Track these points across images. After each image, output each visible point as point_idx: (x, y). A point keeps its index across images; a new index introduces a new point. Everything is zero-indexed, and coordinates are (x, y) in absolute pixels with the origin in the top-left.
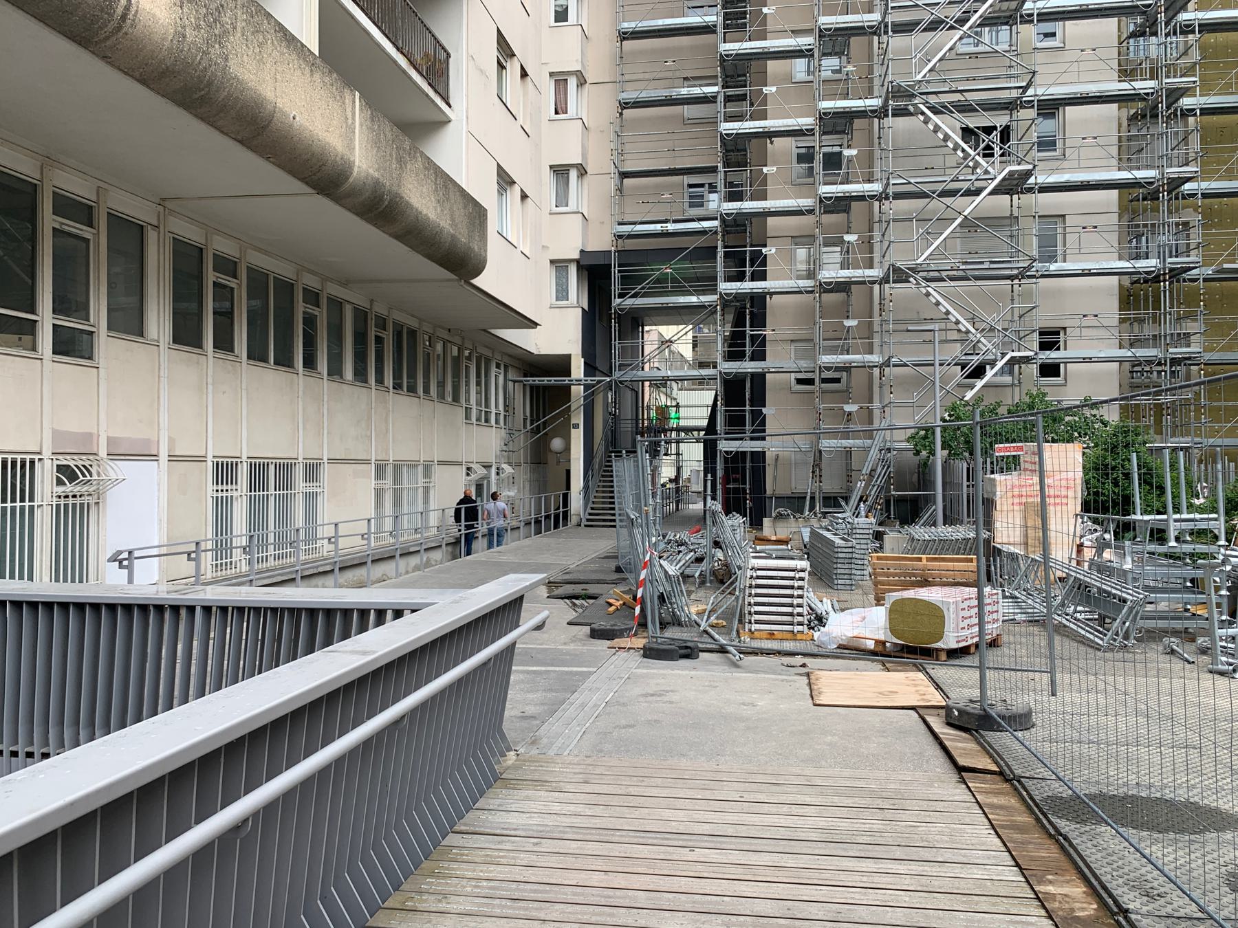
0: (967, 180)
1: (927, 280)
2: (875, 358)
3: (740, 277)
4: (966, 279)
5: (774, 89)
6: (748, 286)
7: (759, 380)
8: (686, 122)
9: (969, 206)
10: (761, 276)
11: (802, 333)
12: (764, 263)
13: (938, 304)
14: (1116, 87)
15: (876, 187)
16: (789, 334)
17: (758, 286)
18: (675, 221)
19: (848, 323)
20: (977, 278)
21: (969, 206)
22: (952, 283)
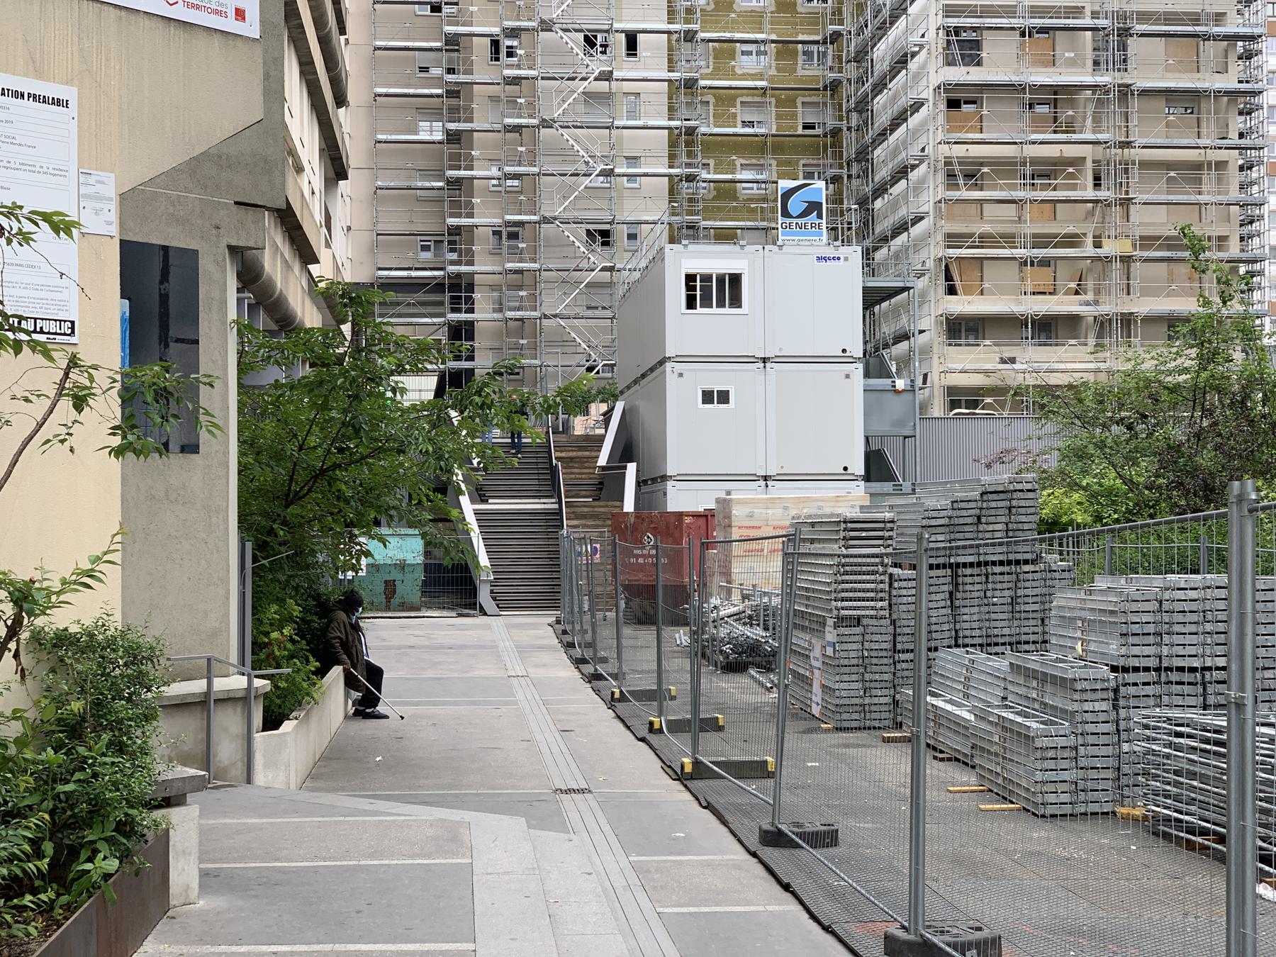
0: (583, 72)
1: (561, 127)
2: (537, 362)
3: (458, 310)
4: (582, 127)
5: (476, 9)
6: (463, 316)
7: (471, 372)
8: (418, 199)
9: (590, 277)
10: (471, 311)
11: (496, 345)
12: (472, 208)
13: (567, 43)
14: (664, 26)
15: (536, 170)
16: (489, 344)
17: (469, 316)
18: (417, 269)
19: (522, 342)
20: (588, 127)
21: (587, 181)
22: (575, 226)
